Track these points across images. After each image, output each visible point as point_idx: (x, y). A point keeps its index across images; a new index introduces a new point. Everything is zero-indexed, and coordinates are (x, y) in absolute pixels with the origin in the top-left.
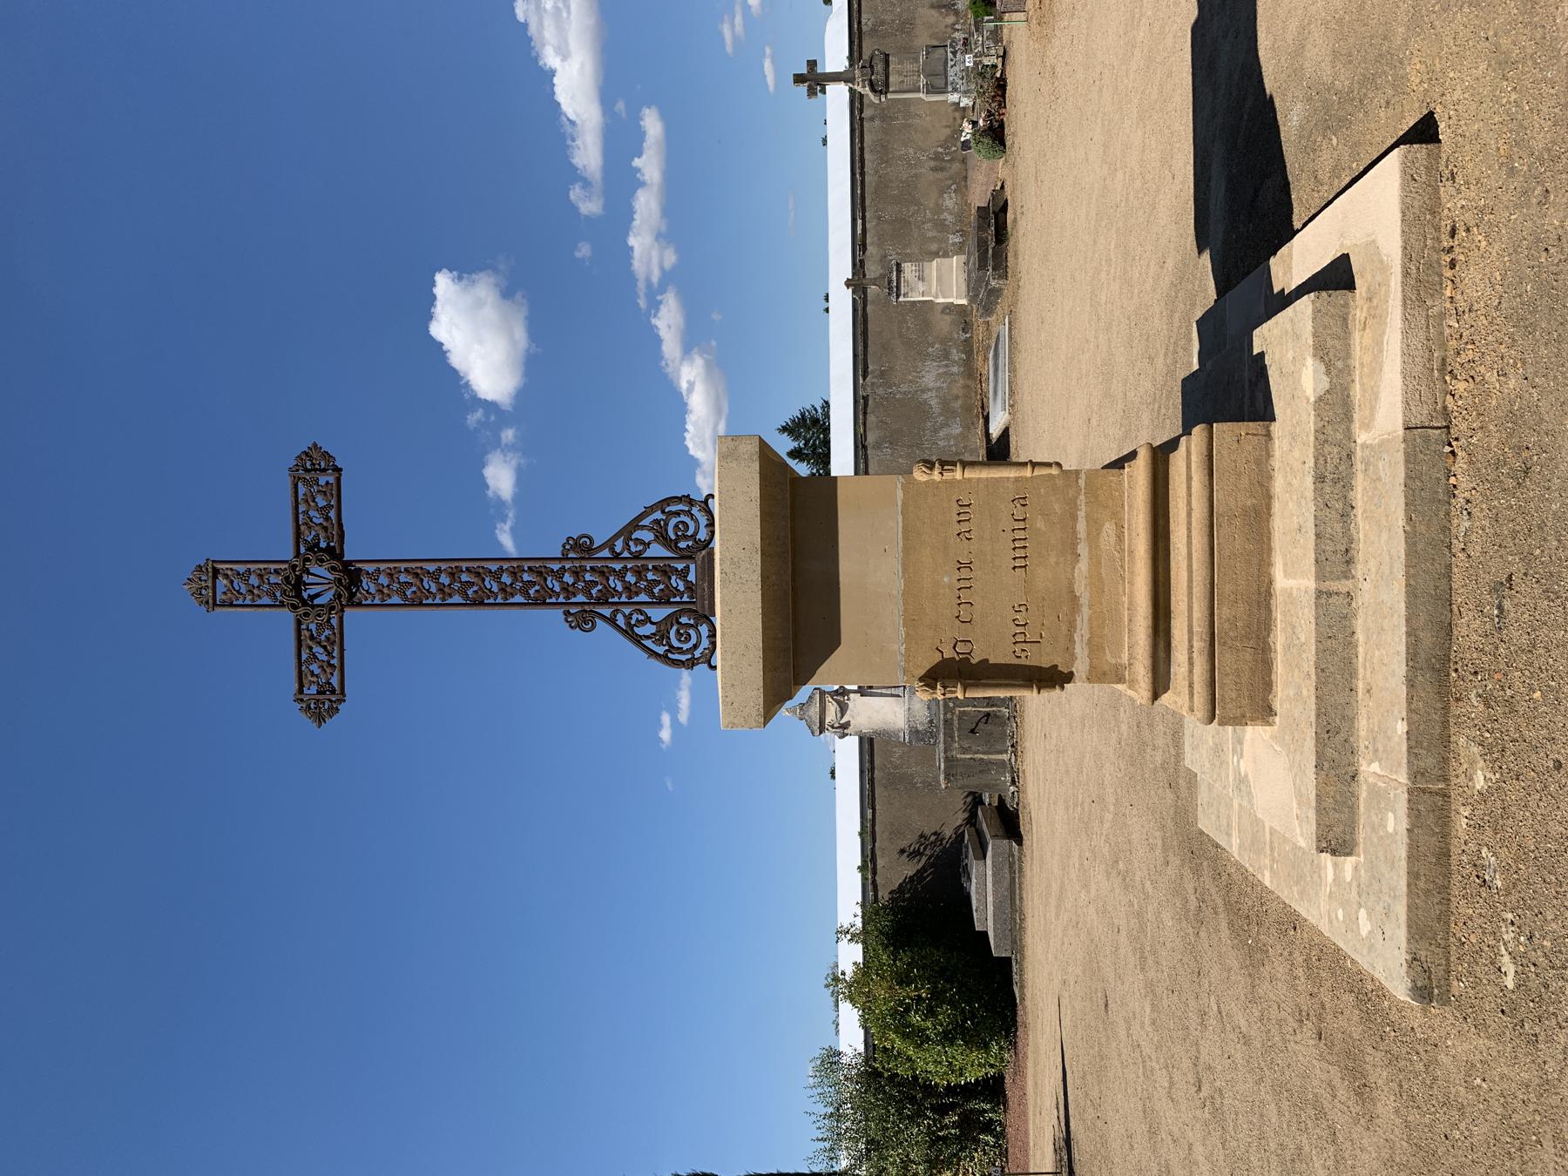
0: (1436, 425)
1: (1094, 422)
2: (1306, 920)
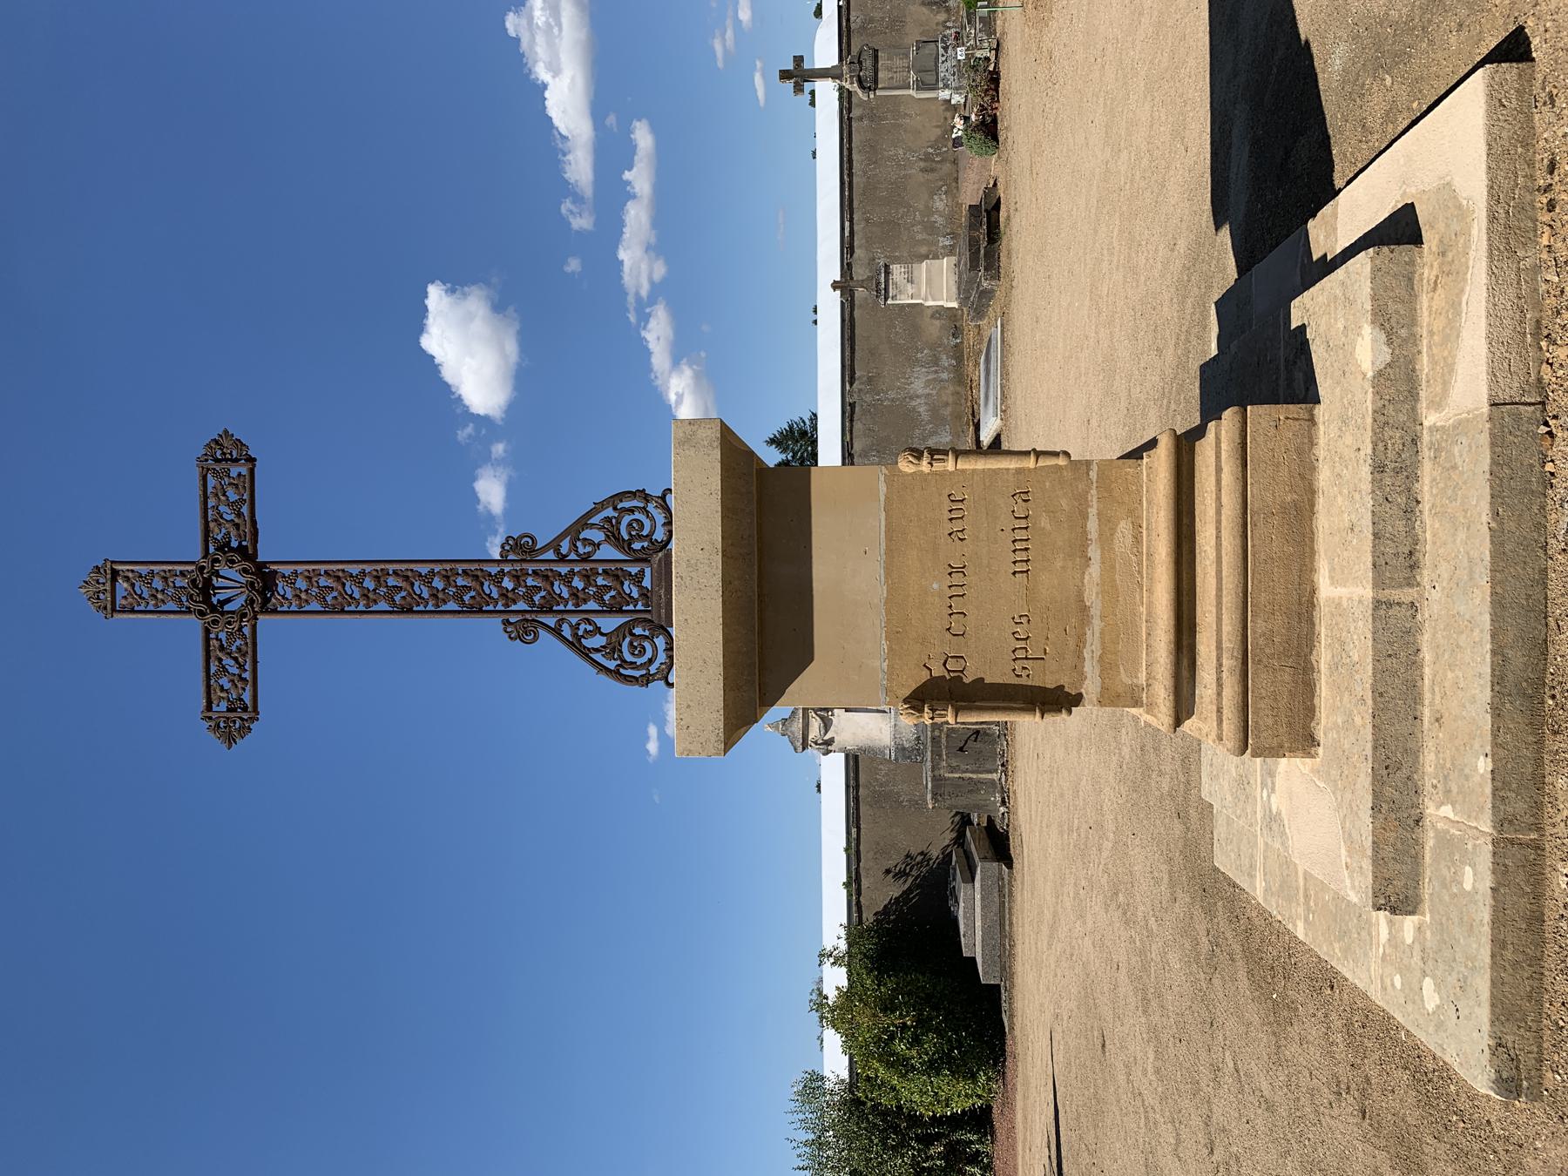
0: (1528, 401)
1: (1094, 423)
2: (1346, 980)
